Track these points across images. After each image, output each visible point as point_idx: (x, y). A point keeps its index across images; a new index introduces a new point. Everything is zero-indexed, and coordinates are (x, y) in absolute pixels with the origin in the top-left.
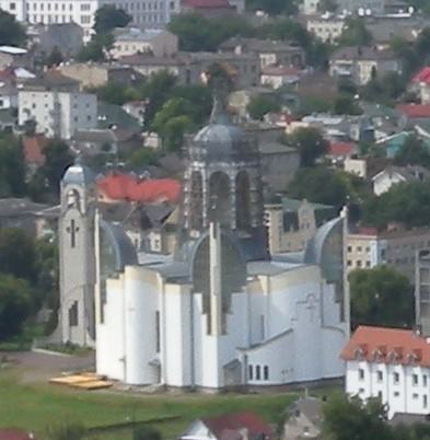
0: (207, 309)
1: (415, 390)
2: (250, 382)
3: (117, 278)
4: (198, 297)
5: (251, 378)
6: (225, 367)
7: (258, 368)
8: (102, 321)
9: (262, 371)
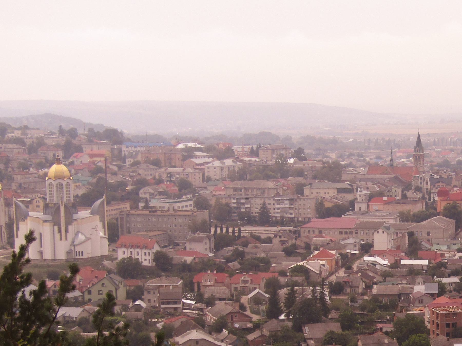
0: (60, 231)
1: (146, 257)
2: (77, 257)
3: (24, 221)
4: (56, 228)
5: (77, 256)
6: (67, 252)
7: (79, 252)
8: (17, 237)
9: (81, 253)
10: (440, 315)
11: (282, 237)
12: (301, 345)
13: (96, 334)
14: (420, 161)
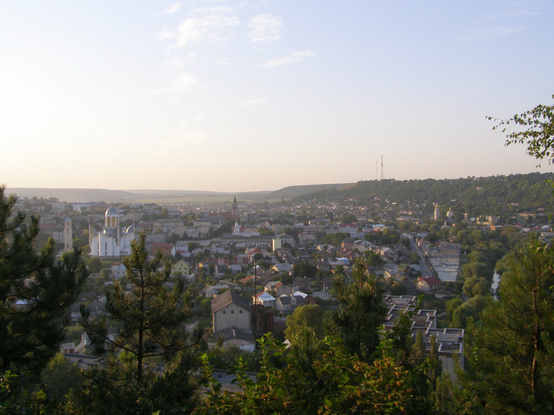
0: (117, 241)
4: (115, 239)
10: (533, 360)
11: (217, 244)
12: (1, 405)
13: (235, 336)
14: (236, 210)
